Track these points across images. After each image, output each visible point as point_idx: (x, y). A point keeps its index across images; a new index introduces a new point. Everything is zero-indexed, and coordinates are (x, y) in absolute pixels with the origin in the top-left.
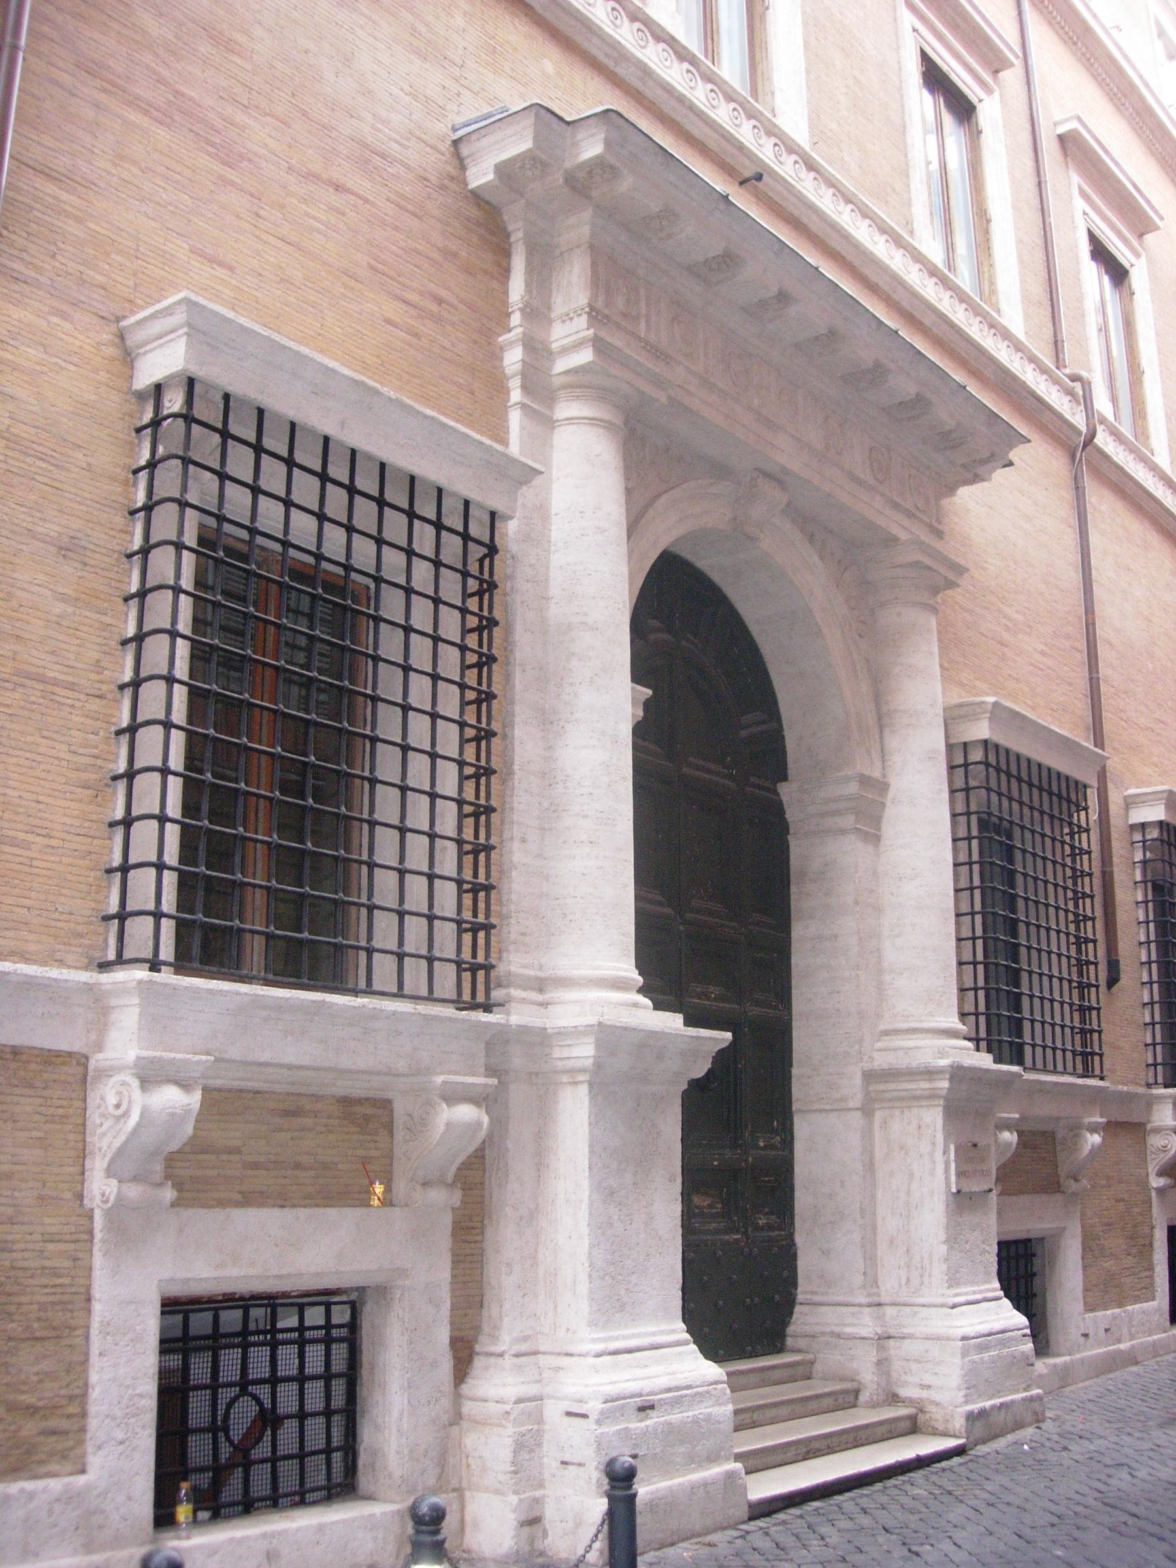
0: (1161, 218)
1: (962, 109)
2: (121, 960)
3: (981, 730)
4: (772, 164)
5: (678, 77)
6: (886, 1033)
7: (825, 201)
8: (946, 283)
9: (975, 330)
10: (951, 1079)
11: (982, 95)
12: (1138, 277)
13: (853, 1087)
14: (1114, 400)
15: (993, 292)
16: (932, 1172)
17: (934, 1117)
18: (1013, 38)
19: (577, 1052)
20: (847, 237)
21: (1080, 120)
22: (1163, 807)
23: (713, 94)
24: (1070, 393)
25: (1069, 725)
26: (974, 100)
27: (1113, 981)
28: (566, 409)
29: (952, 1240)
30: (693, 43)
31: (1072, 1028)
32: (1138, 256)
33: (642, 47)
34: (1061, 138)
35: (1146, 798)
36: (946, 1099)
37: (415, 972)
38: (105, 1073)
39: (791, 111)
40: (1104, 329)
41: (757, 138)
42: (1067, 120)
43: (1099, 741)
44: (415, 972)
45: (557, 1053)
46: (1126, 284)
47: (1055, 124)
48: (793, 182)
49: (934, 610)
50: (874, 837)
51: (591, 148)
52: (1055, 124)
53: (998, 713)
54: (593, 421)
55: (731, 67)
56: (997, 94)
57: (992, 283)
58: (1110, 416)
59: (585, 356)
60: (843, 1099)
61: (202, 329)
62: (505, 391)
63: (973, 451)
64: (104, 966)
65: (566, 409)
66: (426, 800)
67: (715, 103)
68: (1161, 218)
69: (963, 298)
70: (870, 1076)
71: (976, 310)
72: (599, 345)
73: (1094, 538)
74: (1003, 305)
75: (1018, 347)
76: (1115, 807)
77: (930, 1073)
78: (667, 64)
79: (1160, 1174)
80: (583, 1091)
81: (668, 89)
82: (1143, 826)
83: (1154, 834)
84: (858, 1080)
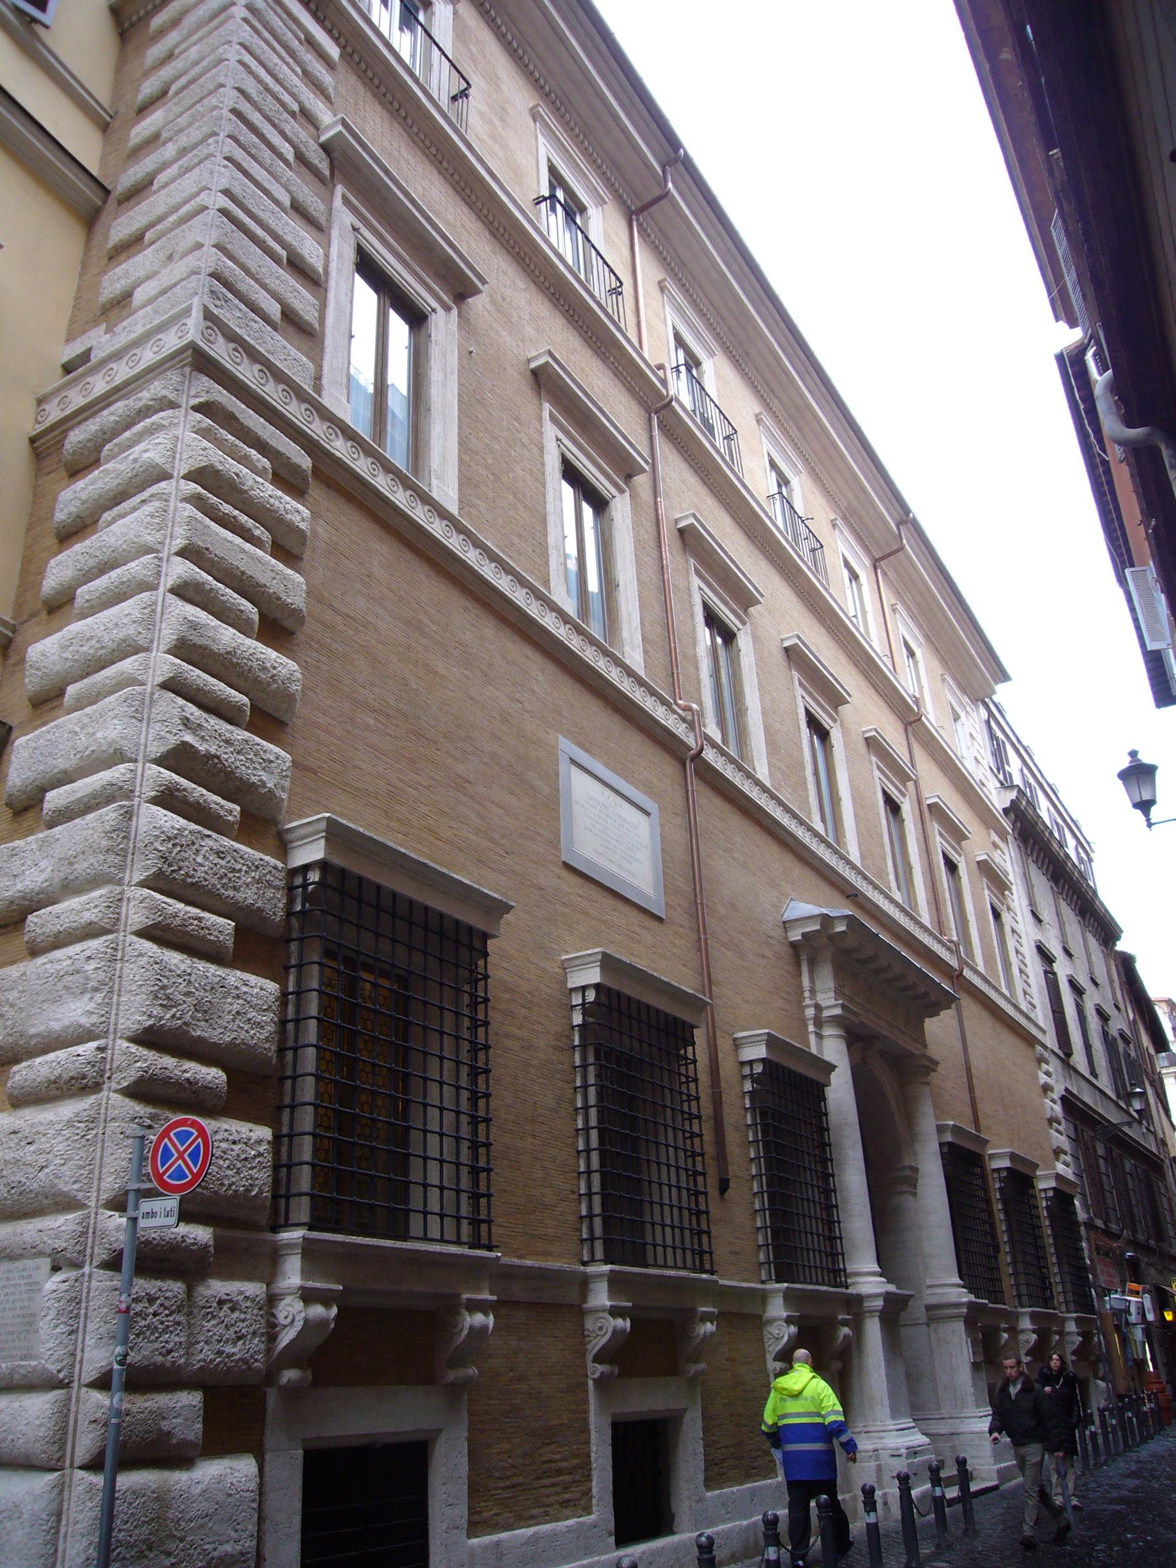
0: (850, 695)
1: (600, 504)
2: (593, 1260)
3: (948, 1138)
4: (228, 366)
5: (384, 483)
6: (930, 1287)
7: (471, 556)
8: (579, 631)
9: (737, 779)
10: (885, 1300)
11: (740, 626)
12: (836, 736)
13: (921, 1315)
14: (823, 820)
15: (916, 905)
16: (962, 1353)
17: (959, 1326)
18: (907, 759)
19: (875, 1304)
20: (877, 906)
21: (799, 638)
22: (598, 969)
23: (210, 331)
24: (949, 949)
25: (684, 980)
26: (827, 727)
27: (724, 1186)
28: (828, 1031)
29: (974, 1385)
30: (363, 428)
31: (691, 1230)
32: (744, 623)
33: (238, 364)
34: (681, 531)
35: (577, 962)
36: (880, 1312)
37: (434, 1224)
38: (771, 1321)
39: (445, 487)
40: (816, 773)
41: (854, 876)
42: (686, 517)
43: (978, 1128)
44: (434, 1224)
45: (865, 1304)
46: (606, 514)
47: (529, 361)
48: (254, 387)
49: (928, 1084)
50: (915, 1195)
51: (841, 928)
52: (529, 361)
53: (1013, 1157)
54: (838, 1036)
55: (926, 918)
56: (627, 493)
57: (916, 900)
58: (718, 738)
59: (838, 1011)
60: (917, 1319)
61: (335, 834)
62: (806, 1026)
63: (937, 1002)
64: (584, 1264)
65: (828, 1031)
66: (437, 1111)
67: (395, 489)
68: (850, 695)
69: (592, 641)
70: (929, 1308)
71: (907, 914)
72: (843, 1006)
73: (966, 1023)
74: (921, 912)
75: (640, 682)
76: (724, 1045)
77: (957, 1305)
78: (395, 489)
79: (1027, 1355)
80: (876, 1320)
81: (827, 865)
82: (751, 1063)
83: (1004, 1174)
84: (923, 1309)
